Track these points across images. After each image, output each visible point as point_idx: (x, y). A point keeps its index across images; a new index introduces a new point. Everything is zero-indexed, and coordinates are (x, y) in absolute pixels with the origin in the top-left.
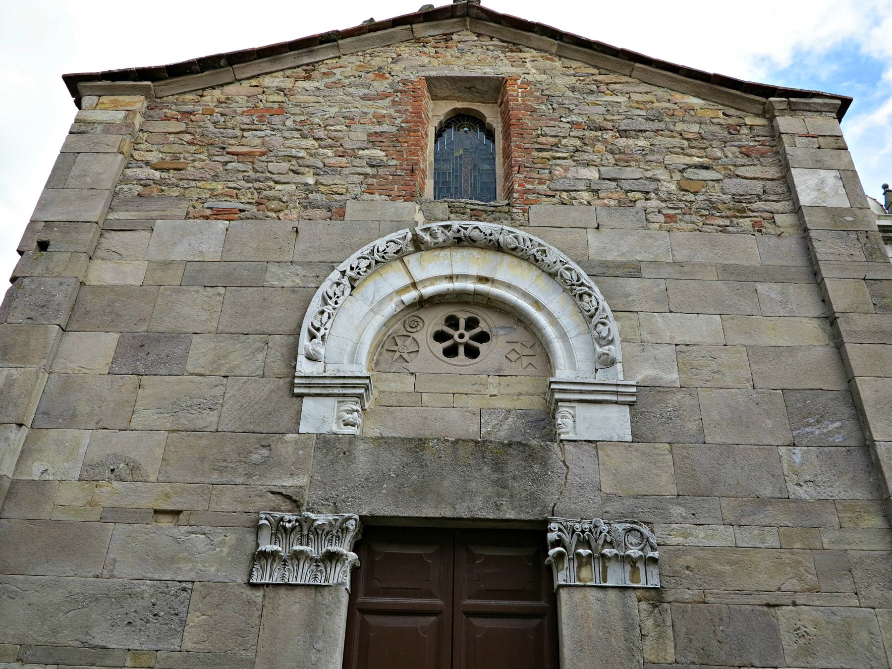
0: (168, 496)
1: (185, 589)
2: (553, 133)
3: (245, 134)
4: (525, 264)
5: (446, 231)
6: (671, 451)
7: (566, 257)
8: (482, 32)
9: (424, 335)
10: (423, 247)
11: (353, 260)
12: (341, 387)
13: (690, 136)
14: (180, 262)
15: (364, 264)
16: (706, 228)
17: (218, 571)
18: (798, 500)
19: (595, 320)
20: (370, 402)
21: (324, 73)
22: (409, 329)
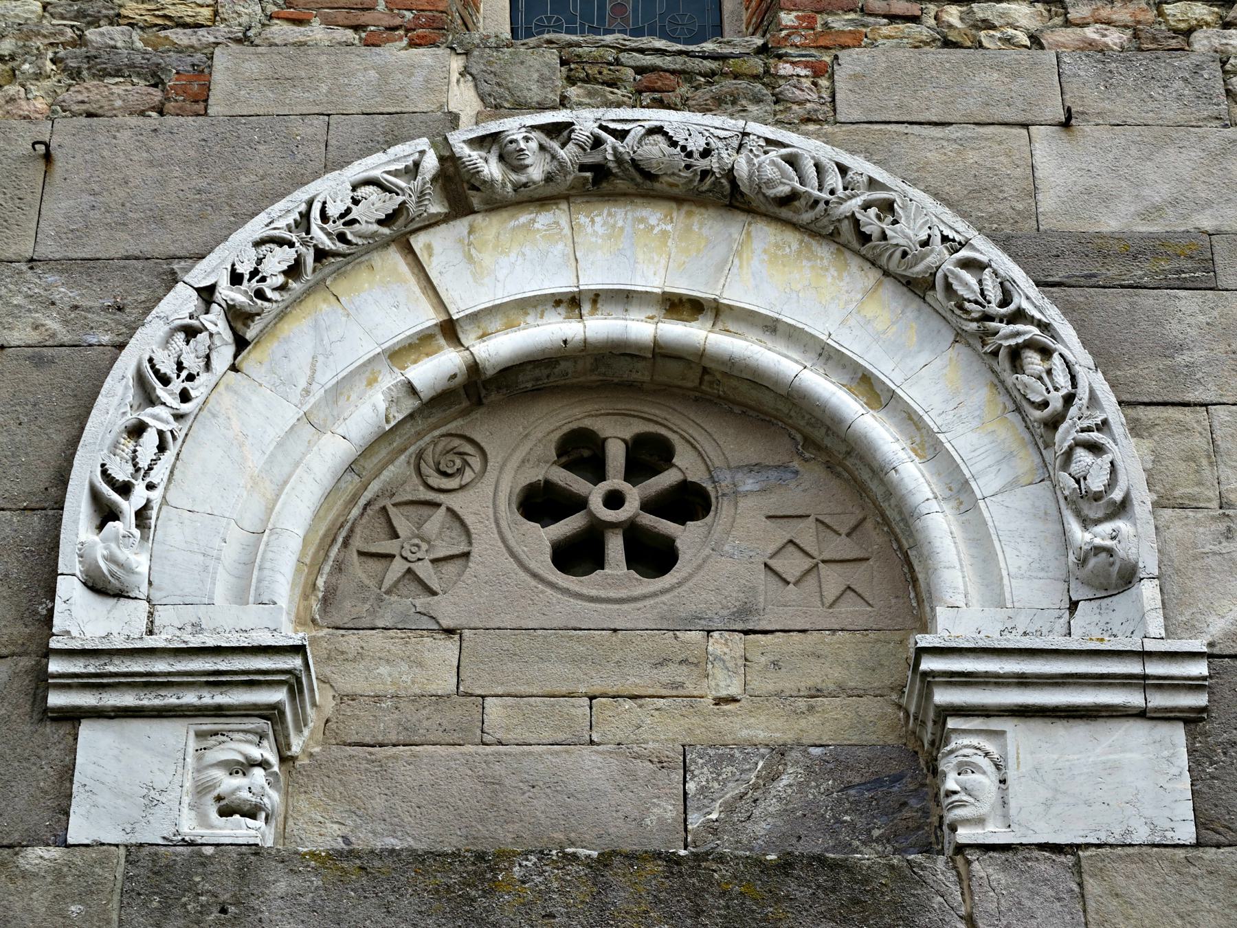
4: (824, 251)
7: (961, 225)
10: (475, 200)
12: (208, 684)
20: (306, 732)
22: (436, 481)
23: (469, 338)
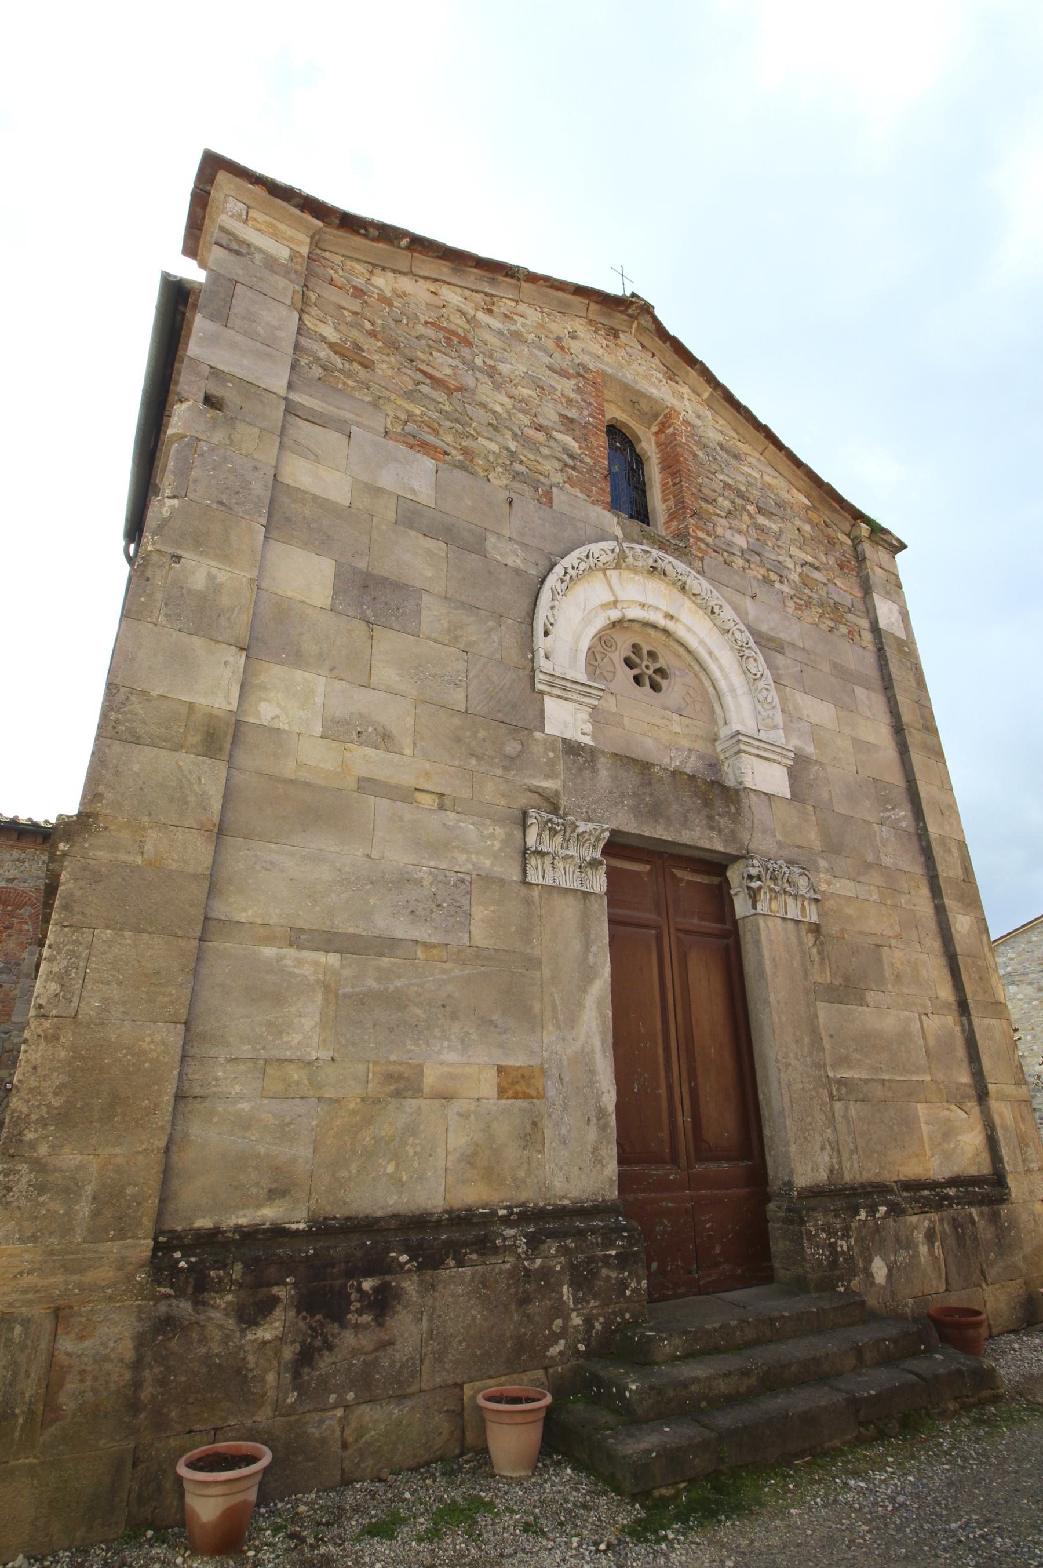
0: (427, 775)
1: (463, 881)
4: (701, 612)
8: (645, 344)
10: (624, 565)
14: (390, 493)
18: (886, 868)
21: (506, 316)
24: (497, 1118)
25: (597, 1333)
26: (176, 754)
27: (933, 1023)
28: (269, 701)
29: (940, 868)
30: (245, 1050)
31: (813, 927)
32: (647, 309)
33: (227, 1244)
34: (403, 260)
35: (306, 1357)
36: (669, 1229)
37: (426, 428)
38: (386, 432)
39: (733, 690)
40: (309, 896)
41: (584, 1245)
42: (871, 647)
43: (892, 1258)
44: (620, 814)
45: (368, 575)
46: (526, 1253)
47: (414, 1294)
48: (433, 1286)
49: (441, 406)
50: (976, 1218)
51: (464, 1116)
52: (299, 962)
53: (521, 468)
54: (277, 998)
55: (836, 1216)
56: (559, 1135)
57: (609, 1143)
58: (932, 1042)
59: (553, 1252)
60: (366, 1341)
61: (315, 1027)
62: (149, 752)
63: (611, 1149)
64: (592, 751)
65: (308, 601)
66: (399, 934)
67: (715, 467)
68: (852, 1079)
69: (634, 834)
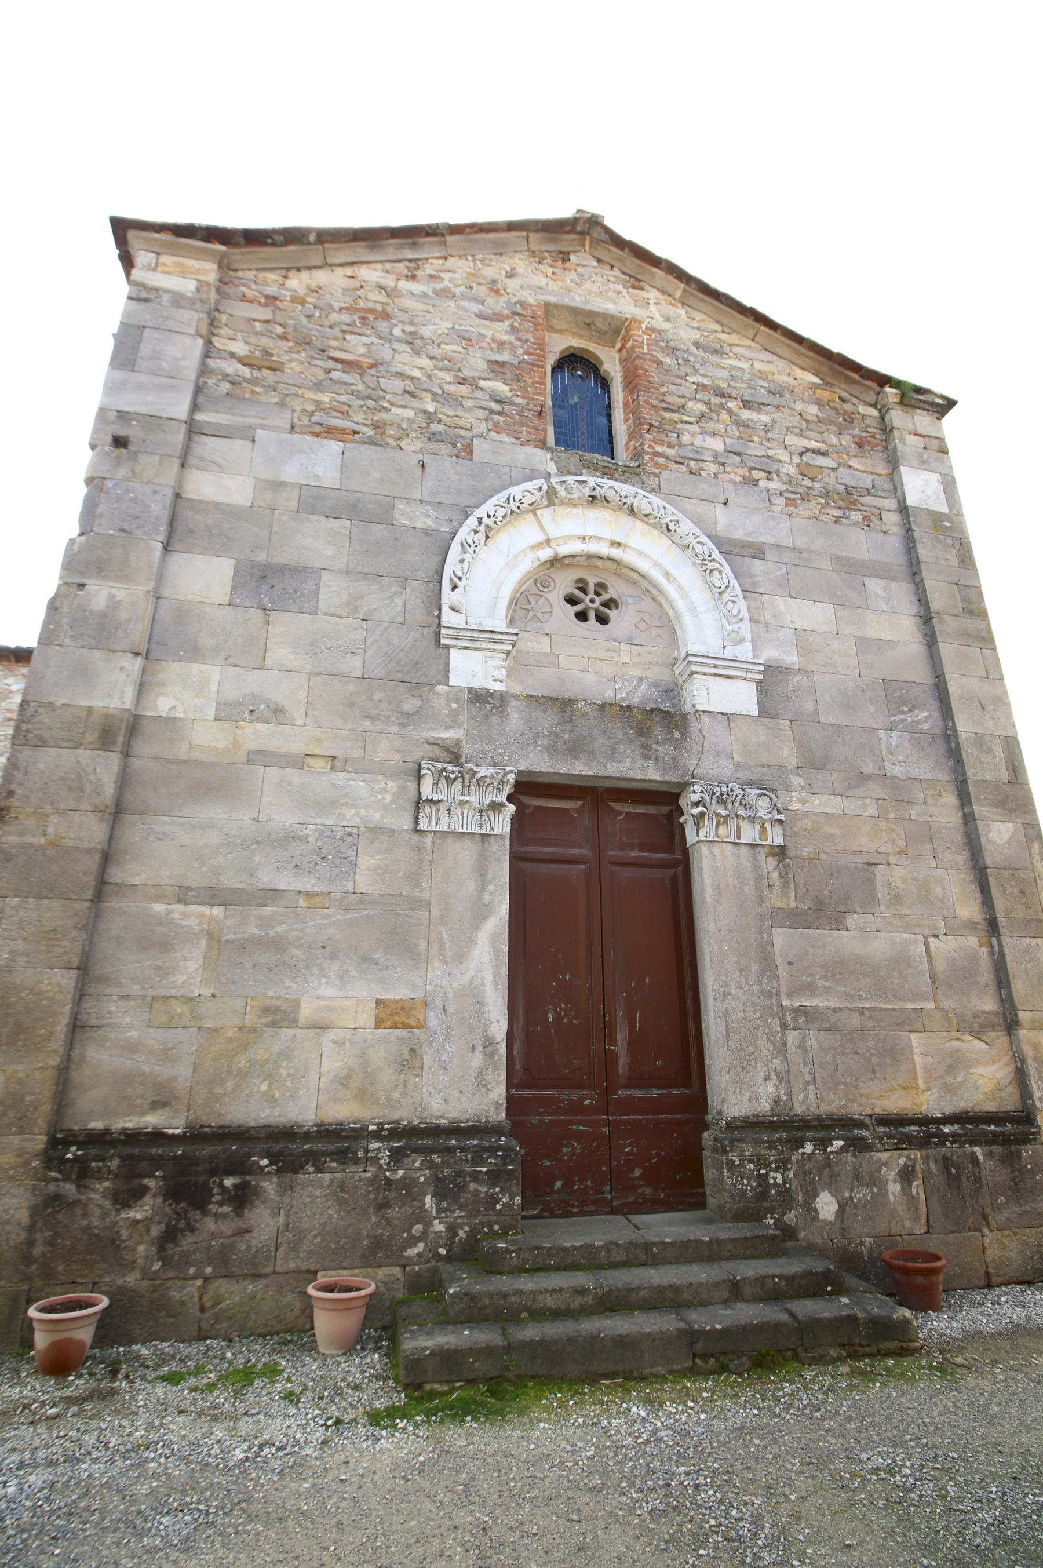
0: (319, 741)
1: (350, 834)
2: (680, 394)
3: (348, 337)
4: (656, 532)
5: (581, 487)
6: (791, 727)
7: (698, 530)
8: (602, 257)
9: (556, 598)
10: (557, 501)
11: (488, 507)
13: (809, 418)
14: (293, 485)
15: (501, 512)
16: (823, 517)
17: (383, 817)
18: (892, 778)
19: (726, 597)
21: (431, 276)
22: (541, 588)
23: (553, 545)
24: (373, 1046)
25: (460, 1240)
26: (76, 751)
27: (945, 947)
28: (167, 695)
29: (970, 772)
30: (136, 989)
31: (777, 850)
32: (594, 222)
33: (113, 1143)
34: (315, 256)
35: (170, 1235)
36: (578, 1151)
37: (335, 414)
38: (292, 428)
39: (693, 610)
40: (197, 859)
41: (452, 1161)
42: (895, 530)
43: (847, 1195)
44: (532, 755)
45: (268, 566)
46: (388, 1164)
47: (272, 1192)
48: (291, 1187)
49: (353, 387)
50: (981, 1158)
51: (340, 1043)
52: (185, 915)
53: (440, 428)
54: (165, 946)
55: (770, 1148)
56: (440, 1061)
57: (496, 1069)
58: (940, 966)
59: (417, 1165)
60: (226, 1227)
61: (198, 969)
62: (53, 752)
63: (499, 1075)
64: (502, 696)
65: (206, 601)
66: (282, 887)
67: (684, 369)
68: (816, 1007)
69: (548, 773)
